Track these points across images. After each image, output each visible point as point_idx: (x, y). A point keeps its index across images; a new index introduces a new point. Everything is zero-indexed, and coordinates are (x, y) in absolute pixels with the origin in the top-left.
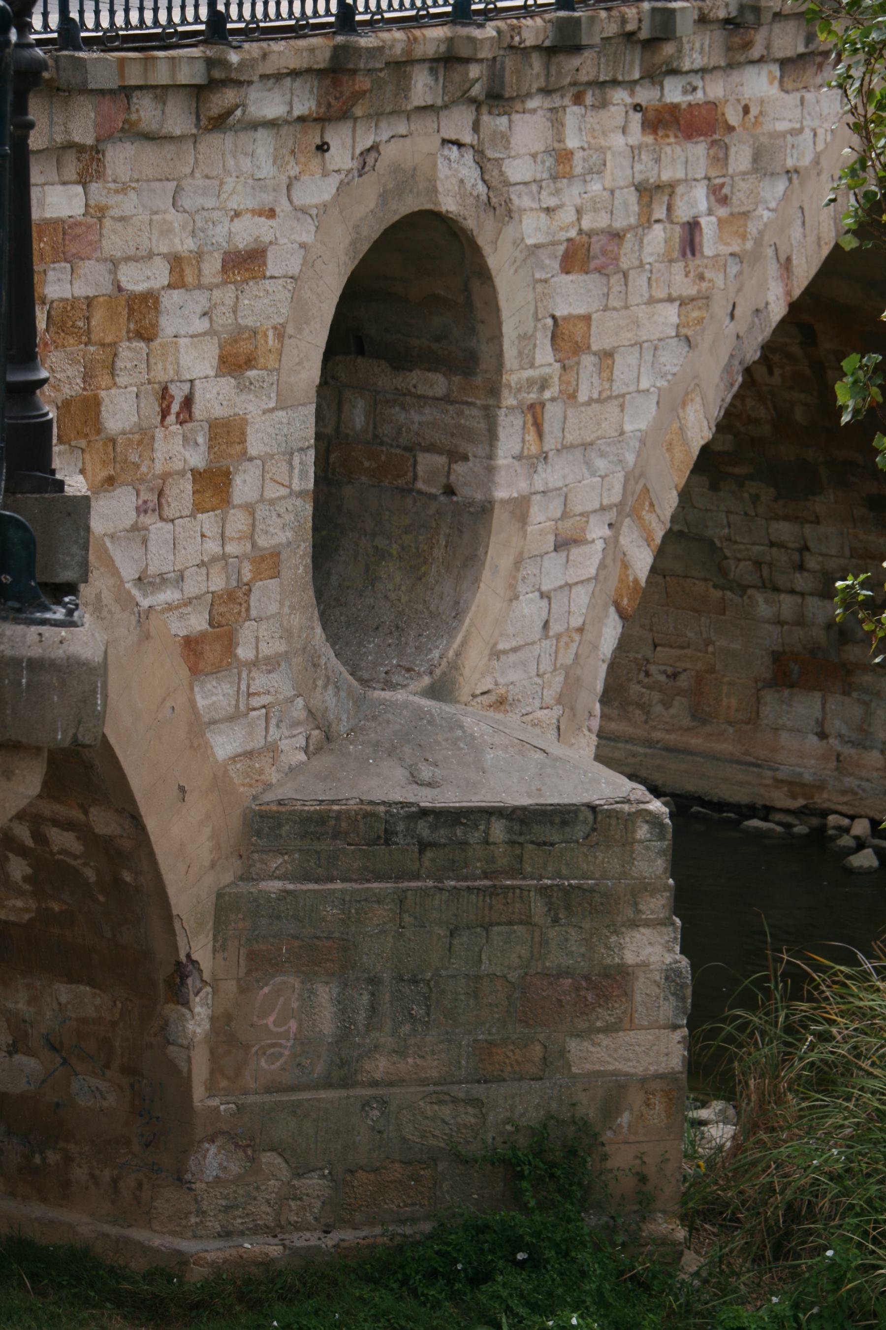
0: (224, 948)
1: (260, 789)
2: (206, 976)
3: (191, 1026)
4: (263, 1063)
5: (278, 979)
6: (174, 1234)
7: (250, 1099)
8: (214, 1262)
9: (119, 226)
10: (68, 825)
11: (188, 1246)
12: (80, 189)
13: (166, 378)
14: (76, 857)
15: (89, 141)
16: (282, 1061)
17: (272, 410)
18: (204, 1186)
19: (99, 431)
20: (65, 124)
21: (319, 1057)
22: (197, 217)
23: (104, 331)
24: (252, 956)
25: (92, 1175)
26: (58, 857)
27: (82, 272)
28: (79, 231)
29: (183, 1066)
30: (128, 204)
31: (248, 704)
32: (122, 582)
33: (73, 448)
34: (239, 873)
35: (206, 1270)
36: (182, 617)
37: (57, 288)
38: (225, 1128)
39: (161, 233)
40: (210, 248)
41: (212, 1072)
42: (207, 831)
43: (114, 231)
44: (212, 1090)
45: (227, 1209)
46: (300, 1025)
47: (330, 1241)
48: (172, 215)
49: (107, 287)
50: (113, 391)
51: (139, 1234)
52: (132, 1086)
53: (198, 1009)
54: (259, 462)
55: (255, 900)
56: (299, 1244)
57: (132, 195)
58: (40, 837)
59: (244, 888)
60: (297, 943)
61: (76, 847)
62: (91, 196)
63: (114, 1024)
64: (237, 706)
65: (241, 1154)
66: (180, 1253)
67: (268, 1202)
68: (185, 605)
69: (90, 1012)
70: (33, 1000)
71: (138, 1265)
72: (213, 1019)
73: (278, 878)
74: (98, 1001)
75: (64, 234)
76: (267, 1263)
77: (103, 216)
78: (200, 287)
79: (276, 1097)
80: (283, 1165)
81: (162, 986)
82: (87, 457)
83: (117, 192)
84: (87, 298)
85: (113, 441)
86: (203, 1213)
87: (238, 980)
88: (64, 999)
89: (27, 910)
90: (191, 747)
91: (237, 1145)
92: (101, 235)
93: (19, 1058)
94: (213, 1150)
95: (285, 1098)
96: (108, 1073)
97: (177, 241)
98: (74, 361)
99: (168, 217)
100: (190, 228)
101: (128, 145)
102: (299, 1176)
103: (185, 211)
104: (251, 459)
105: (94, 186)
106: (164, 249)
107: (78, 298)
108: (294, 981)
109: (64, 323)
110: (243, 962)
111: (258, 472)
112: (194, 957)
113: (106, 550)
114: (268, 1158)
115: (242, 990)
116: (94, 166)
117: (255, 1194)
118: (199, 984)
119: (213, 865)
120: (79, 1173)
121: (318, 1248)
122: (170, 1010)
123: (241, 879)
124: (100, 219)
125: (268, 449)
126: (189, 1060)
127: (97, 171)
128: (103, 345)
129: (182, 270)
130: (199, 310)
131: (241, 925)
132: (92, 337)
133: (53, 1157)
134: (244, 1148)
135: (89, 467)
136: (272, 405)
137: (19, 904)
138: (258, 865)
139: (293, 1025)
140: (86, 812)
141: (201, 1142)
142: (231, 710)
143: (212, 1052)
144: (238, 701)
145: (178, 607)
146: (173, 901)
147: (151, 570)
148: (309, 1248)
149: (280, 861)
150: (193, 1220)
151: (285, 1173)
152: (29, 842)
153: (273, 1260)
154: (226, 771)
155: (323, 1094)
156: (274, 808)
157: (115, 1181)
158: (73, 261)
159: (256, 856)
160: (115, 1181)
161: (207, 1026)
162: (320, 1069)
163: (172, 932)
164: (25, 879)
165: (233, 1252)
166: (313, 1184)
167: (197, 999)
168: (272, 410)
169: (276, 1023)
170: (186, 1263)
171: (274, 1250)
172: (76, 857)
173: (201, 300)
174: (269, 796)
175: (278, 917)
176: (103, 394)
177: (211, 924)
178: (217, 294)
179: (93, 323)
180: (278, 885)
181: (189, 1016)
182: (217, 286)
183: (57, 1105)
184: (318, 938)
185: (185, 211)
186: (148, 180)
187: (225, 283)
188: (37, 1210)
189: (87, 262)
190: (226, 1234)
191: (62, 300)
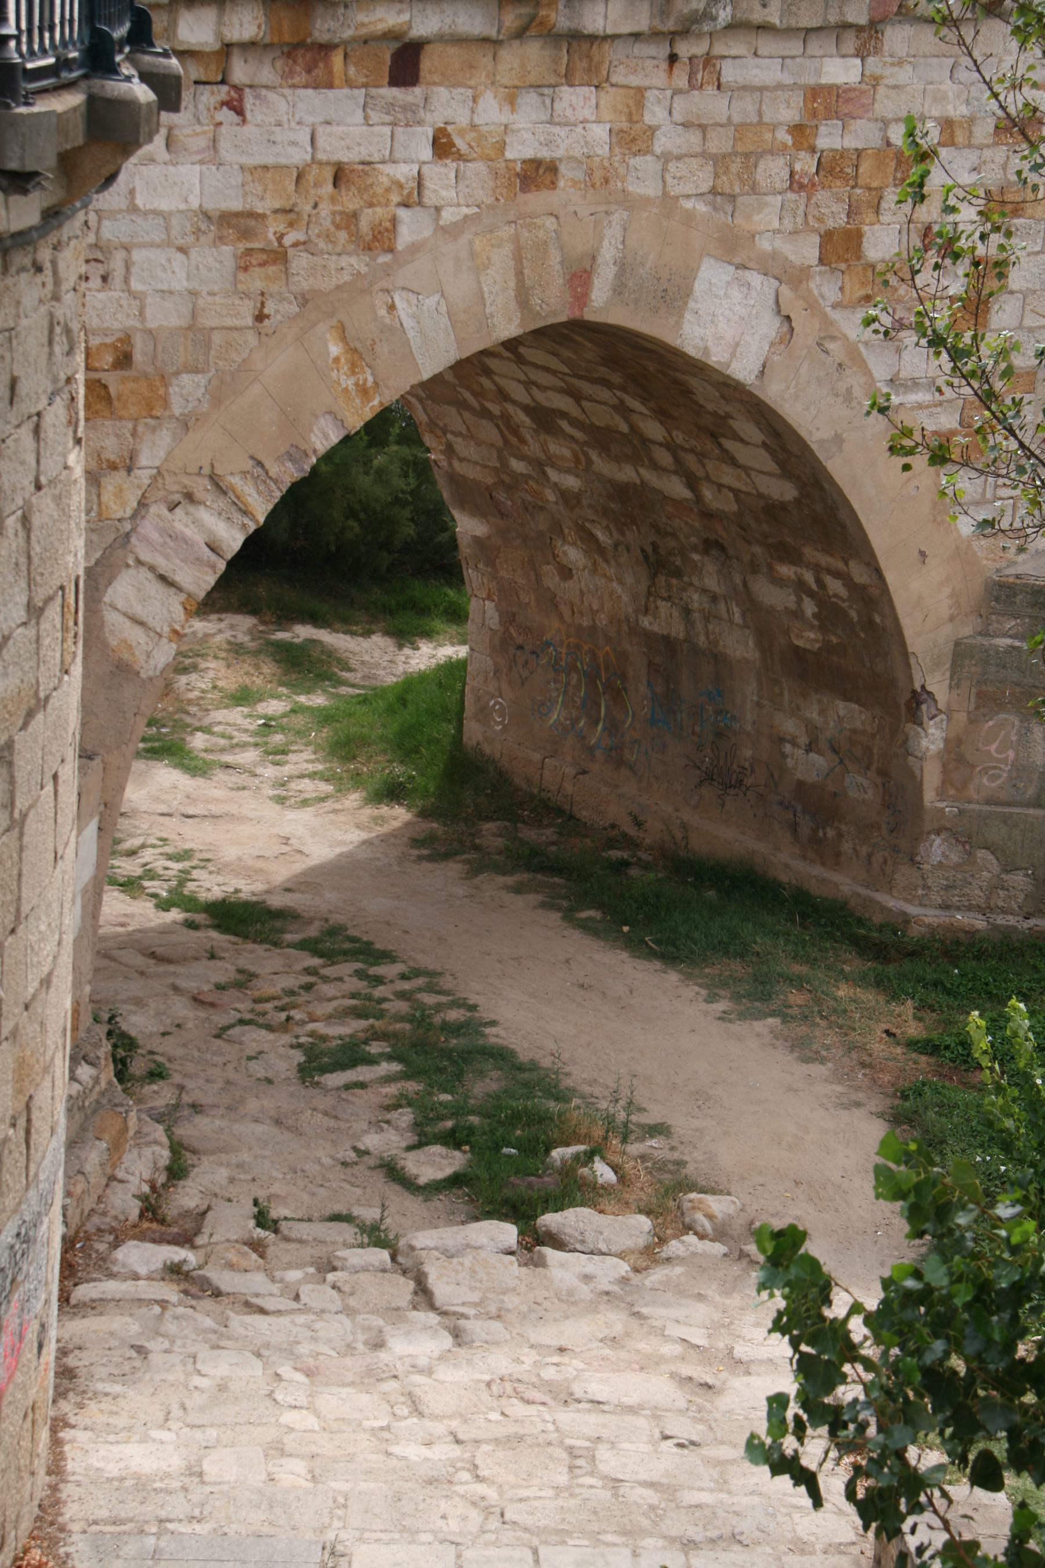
0: (958, 686)
1: (1004, 565)
2: (941, 705)
3: (924, 743)
4: (985, 781)
5: (1002, 716)
6: (906, 900)
7: (972, 806)
8: (930, 925)
9: (893, 93)
10: (837, 574)
11: (912, 910)
12: (858, 61)
13: (929, 219)
14: (844, 601)
15: (863, 21)
16: (1000, 781)
17: (1037, 253)
18: (929, 867)
19: (859, 258)
20: (840, 8)
21: (1031, 782)
22: (972, 89)
23: (870, 177)
24: (980, 695)
25: (855, 850)
26: (834, 600)
27: (853, 128)
28: (852, 95)
29: (917, 772)
30: (904, 75)
31: (995, 494)
32: (873, 381)
33: (833, 270)
34: (979, 629)
35: (923, 930)
36: (931, 415)
37: (827, 140)
38: (948, 825)
39: (935, 99)
40: (983, 114)
41: (944, 782)
42: (947, 591)
43: (887, 97)
44: (941, 794)
45: (947, 888)
46: (1017, 755)
47: (1026, 925)
48: (948, 86)
49: (876, 141)
50: (876, 227)
51: (881, 897)
52: (884, 785)
53: (931, 731)
54: (1020, 296)
55: (986, 651)
56: (999, 922)
57: (909, 68)
58: (819, 582)
59: (980, 640)
60: (1018, 689)
61: (844, 593)
62: (867, 67)
63: (873, 735)
64: (984, 494)
65: (960, 847)
66: (905, 914)
67: (981, 888)
68: (935, 406)
69: (858, 725)
70: (822, 712)
71: (878, 919)
72: (946, 740)
73: (1010, 637)
74: (863, 717)
75: (838, 96)
76: (972, 933)
77: (878, 84)
78: (970, 146)
79: (993, 808)
80: (994, 861)
81: (903, 708)
82: (847, 278)
83: (893, 64)
84: (857, 150)
85: (873, 267)
86: (926, 887)
87: (969, 713)
88: (841, 713)
89: (817, 641)
90: (935, 520)
91: (957, 840)
92: (874, 99)
93: (813, 756)
94: (938, 841)
95: (999, 809)
96: (869, 773)
97: (950, 107)
98: (839, 200)
99: (943, 87)
100: (965, 97)
101: (907, 27)
102: (1008, 872)
103: (960, 83)
104: (1012, 292)
105: (870, 60)
106: (936, 113)
107: (848, 150)
108: (1014, 719)
109: (833, 169)
110: (973, 699)
111: (1019, 304)
112: (929, 688)
113: (860, 354)
114: (982, 855)
115: (971, 721)
116: (873, 42)
117: (970, 880)
118: (934, 712)
119: (951, 619)
120: (847, 847)
121: (1015, 928)
122: (910, 728)
123: (980, 634)
124: (874, 87)
125: (1030, 286)
126: (922, 769)
127: (875, 48)
128: (869, 189)
129: (953, 132)
130: (968, 165)
131: (973, 669)
132: (859, 182)
133: (831, 833)
134: (964, 844)
135: (847, 287)
136: (1037, 249)
137: (812, 635)
138: (995, 625)
139: (1011, 754)
140: (847, 564)
141: (929, 833)
142: (978, 497)
143: (944, 766)
144: (984, 490)
145: (927, 407)
146: (908, 641)
147: (903, 374)
148: (1007, 927)
149: (1013, 623)
150: (920, 892)
151: (995, 867)
152: (814, 587)
153: (978, 931)
154: (969, 545)
155: (1031, 811)
156: (1011, 580)
157: (870, 856)
158: (845, 119)
159: (994, 617)
160: (870, 856)
161: (941, 745)
162: (1031, 791)
163: (908, 666)
164: (814, 615)
165: (947, 920)
166: (1018, 879)
167: (932, 723)
168: (1037, 253)
169: (997, 751)
170: (908, 922)
171: (980, 923)
172: (844, 601)
173: (972, 157)
174: (1012, 571)
175: (1004, 667)
176: (866, 228)
177: (948, 665)
178: (987, 153)
179: (861, 170)
180: (1009, 641)
181: (923, 734)
182: (988, 146)
183: (835, 794)
184: (1036, 687)
185: (960, 83)
186: (926, 56)
187: (996, 144)
188: (817, 870)
189: (858, 121)
190: (946, 907)
191: (832, 150)
